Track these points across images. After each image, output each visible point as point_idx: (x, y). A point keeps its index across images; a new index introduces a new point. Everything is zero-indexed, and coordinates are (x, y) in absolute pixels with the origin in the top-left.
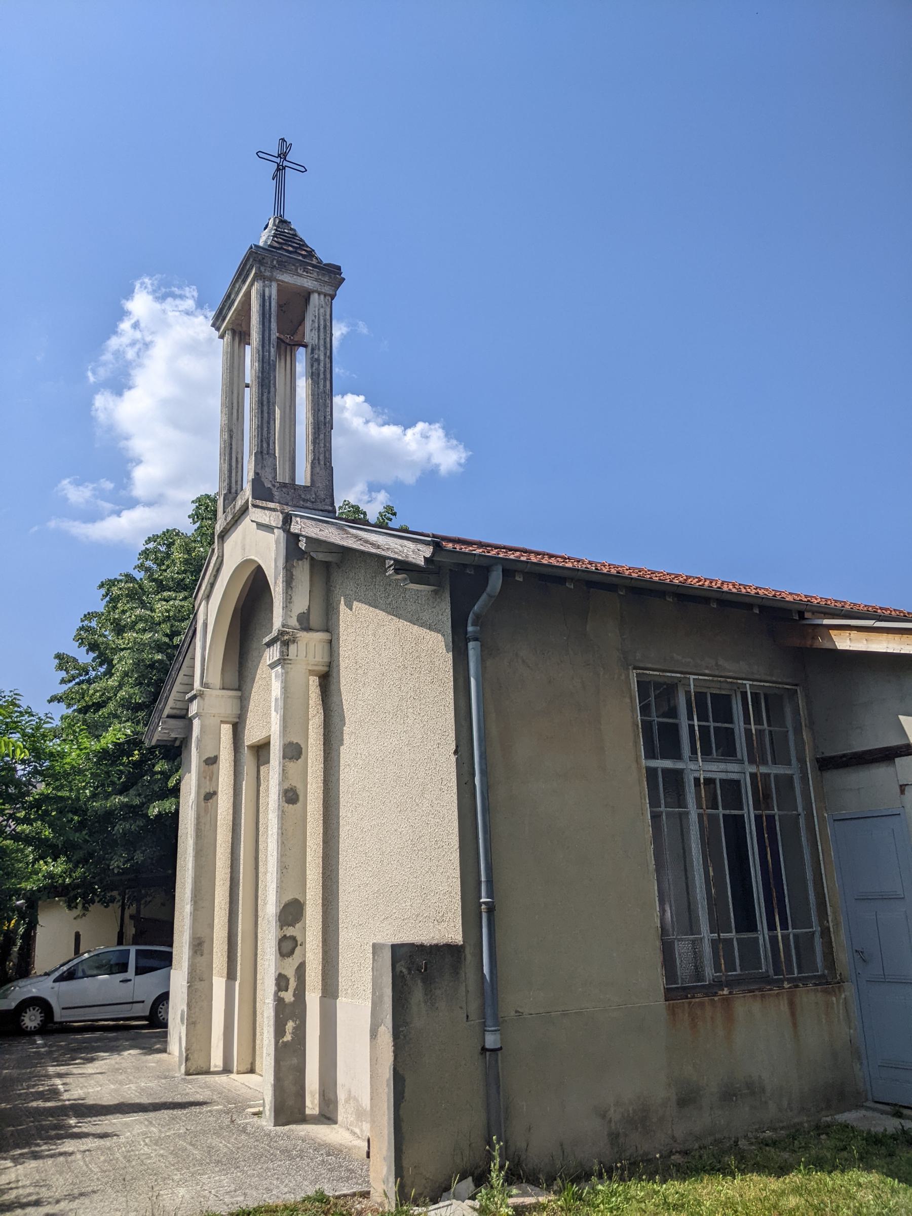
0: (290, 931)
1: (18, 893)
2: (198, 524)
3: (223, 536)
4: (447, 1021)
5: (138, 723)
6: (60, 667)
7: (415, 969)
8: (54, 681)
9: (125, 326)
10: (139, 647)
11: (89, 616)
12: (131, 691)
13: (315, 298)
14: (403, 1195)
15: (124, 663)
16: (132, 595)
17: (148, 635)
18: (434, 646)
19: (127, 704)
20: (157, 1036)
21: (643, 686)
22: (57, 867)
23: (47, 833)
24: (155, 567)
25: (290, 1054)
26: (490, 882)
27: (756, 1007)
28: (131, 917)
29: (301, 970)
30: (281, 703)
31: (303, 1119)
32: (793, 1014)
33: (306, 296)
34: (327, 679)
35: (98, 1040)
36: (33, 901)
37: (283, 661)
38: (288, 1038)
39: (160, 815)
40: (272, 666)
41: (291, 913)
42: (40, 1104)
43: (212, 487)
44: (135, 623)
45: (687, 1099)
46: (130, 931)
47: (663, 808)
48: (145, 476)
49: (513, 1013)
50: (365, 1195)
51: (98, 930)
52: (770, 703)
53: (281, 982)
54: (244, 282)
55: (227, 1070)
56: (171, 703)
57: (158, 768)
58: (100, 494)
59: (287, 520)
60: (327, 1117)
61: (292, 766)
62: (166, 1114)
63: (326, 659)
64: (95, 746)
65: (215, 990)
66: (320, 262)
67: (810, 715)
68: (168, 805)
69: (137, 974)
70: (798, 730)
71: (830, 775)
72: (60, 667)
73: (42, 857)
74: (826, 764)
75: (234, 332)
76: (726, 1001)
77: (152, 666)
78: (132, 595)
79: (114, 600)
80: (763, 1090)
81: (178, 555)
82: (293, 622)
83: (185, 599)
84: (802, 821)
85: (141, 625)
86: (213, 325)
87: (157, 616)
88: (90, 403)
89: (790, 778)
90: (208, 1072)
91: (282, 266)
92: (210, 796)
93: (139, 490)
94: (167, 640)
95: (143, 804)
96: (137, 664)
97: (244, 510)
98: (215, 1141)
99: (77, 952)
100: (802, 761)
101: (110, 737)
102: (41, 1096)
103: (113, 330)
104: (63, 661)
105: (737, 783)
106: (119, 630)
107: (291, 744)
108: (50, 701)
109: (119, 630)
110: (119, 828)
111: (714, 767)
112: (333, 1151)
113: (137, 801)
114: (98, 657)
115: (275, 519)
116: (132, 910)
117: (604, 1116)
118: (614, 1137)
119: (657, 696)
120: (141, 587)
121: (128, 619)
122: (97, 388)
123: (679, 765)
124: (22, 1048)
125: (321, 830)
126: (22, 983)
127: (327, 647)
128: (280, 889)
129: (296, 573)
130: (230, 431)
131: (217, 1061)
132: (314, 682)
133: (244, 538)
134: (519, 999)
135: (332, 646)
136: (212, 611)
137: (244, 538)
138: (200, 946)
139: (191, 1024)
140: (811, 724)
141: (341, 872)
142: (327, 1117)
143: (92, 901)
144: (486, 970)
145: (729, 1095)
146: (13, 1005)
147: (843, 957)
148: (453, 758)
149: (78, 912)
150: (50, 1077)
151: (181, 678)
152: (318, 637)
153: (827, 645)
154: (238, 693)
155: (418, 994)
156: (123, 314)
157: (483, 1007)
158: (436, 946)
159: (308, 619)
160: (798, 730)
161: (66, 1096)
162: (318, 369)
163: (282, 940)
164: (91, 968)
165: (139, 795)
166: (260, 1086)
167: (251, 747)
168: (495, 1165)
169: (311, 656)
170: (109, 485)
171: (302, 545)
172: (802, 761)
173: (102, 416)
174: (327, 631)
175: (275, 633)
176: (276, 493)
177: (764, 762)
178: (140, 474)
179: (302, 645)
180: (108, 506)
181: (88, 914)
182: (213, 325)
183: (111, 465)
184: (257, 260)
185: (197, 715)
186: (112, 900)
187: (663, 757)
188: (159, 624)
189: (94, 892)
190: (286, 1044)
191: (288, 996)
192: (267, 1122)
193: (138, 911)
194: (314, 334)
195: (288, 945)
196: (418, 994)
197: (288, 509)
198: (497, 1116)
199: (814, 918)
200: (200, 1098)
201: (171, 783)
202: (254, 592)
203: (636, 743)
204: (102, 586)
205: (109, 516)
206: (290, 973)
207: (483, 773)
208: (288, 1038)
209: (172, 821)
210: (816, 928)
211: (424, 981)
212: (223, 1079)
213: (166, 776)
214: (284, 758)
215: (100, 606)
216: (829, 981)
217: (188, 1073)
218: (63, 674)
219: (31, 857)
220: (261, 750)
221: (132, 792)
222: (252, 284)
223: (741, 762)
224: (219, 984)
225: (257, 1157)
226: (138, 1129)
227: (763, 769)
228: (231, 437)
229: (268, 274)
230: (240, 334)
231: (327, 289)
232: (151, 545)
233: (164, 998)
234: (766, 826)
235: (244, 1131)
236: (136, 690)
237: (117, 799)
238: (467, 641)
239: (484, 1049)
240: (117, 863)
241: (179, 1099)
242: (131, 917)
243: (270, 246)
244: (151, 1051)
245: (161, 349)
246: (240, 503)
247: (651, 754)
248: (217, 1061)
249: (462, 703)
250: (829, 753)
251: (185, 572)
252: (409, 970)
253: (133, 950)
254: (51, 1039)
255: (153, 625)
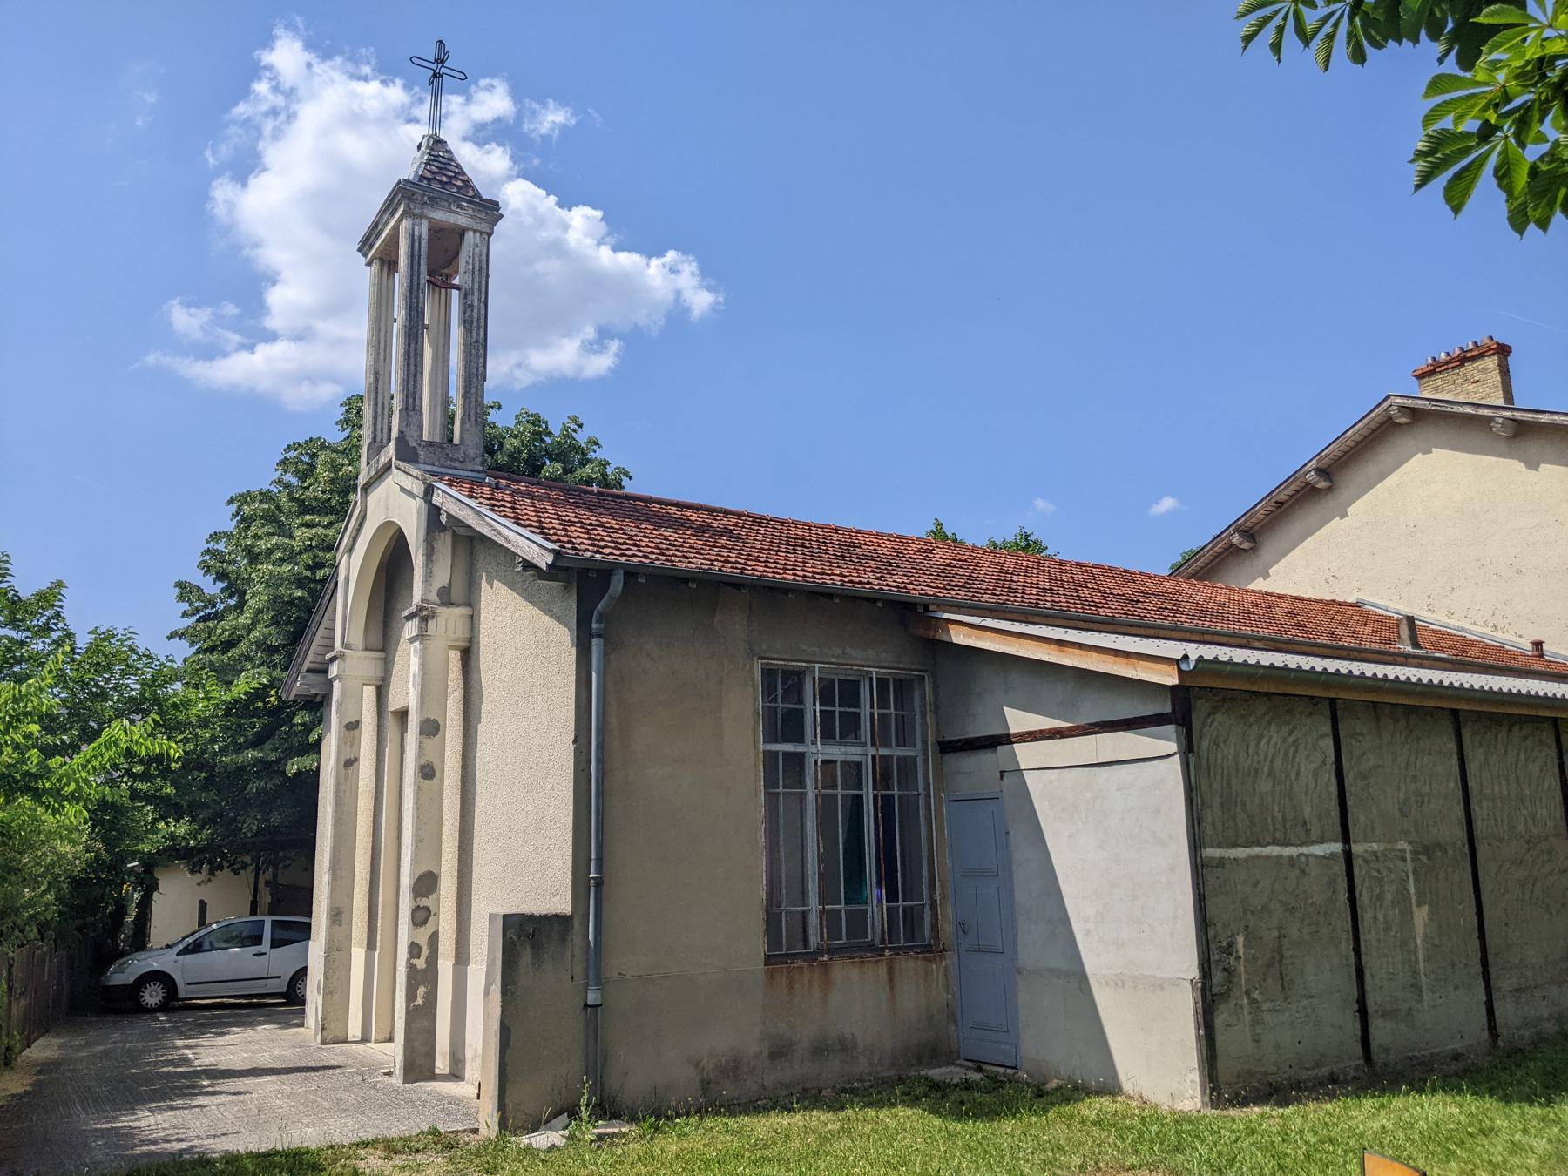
0: (423, 902)
1: (133, 855)
2: (347, 432)
3: (366, 488)
4: (557, 984)
5: (275, 667)
6: (182, 598)
7: (525, 936)
8: (175, 615)
9: (262, 87)
10: (274, 581)
11: (216, 537)
12: (266, 631)
13: (469, 236)
14: (503, 1124)
15: (257, 598)
16: (269, 518)
17: (286, 568)
18: (561, 639)
19: (261, 644)
20: (293, 1012)
21: (768, 673)
22: (181, 828)
23: (169, 790)
24: (295, 481)
25: (421, 1018)
26: (600, 859)
27: (854, 972)
28: (267, 883)
29: (434, 939)
30: (418, 680)
31: (433, 1077)
32: (891, 980)
33: (462, 232)
34: (468, 655)
35: (230, 1016)
36: (150, 864)
37: (422, 636)
38: (419, 1001)
39: (299, 772)
40: (412, 640)
41: (426, 884)
42: (172, 1069)
43: (362, 385)
44: (270, 552)
45: (780, 1051)
46: (266, 898)
47: (781, 789)
48: (287, 299)
49: (616, 975)
50: (475, 1131)
51: (228, 899)
52: (897, 689)
53: (414, 950)
54: (392, 214)
55: (365, 1039)
56: (310, 656)
57: (297, 720)
58: (218, 321)
59: (429, 490)
60: (456, 1075)
61: (428, 742)
62: (299, 1076)
63: (467, 635)
64: (227, 697)
65: (350, 959)
66: (477, 195)
67: (936, 699)
68: (307, 762)
69: (272, 946)
70: (924, 715)
71: (947, 757)
72: (182, 598)
73: (163, 818)
74: (948, 747)
75: (382, 261)
76: (825, 965)
77: (292, 602)
78: (269, 518)
79: (246, 522)
80: (855, 1046)
81: (323, 474)
82: (434, 597)
83: (330, 524)
84: (922, 802)
85: (278, 555)
86: (359, 250)
87: (297, 545)
88: (204, 196)
89: (914, 759)
90: (345, 1042)
91: (434, 202)
92: (351, 763)
93: (273, 322)
94: (308, 573)
95: (279, 760)
96: (275, 599)
97: (387, 468)
98: (345, 1095)
99: (202, 922)
100: (925, 742)
101: (242, 686)
102: (172, 1063)
103: (244, 93)
104: (185, 590)
105: (858, 765)
106: (254, 558)
107: (428, 720)
108: (169, 638)
109: (254, 558)
110: (253, 787)
111: (835, 749)
112: (454, 1100)
113: (273, 757)
114: (227, 588)
115: (418, 488)
116: (268, 875)
117: (697, 1066)
118: (705, 1084)
119: (782, 684)
120: (278, 508)
121: (263, 545)
122: (218, 172)
123: (800, 749)
124: (143, 1023)
125: (458, 804)
126: (141, 955)
127: (468, 621)
128: (415, 861)
129: (438, 545)
130: (377, 373)
131: (355, 1031)
132: (454, 656)
133: (387, 497)
134: (615, 965)
135: (473, 620)
136: (353, 567)
137: (387, 497)
138: (338, 916)
139: (328, 992)
140: (936, 709)
141: (475, 846)
142: (456, 1075)
143: (221, 868)
144: (591, 937)
145: (821, 1050)
146: (132, 980)
147: (948, 928)
148: (572, 747)
149: (199, 877)
150: (178, 1048)
151: (317, 641)
152: (459, 612)
153: (945, 638)
154: (382, 655)
155: (526, 957)
156: (256, 71)
157: (586, 970)
158: (546, 916)
159: (449, 594)
160: (924, 715)
161: (197, 1063)
162: (471, 317)
163: (416, 910)
164: (218, 940)
165: (276, 749)
166: (393, 1052)
167: (395, 713)
168: (583, 1101)
169: (451, 634)
170: (231, 309)
171: (443, 518)
172: (925, 742)
173: (220, 210)
174: (469, 605)
175: (413, 609)
176: (421, 452)
177: (886, 744)
178: (276, 297)
179: (441, 620)
180: (237, 338)
181: (215, 881)
182: (359, 250)
183: (240, 290)
184: (405, 195)
185: (337, 677)
186: (245, 866)
187: (785, 741)
188: (300, 553)
189: (224, 857)
190: (416, 1007)
191: (420, 963)
192: (397, 1081)
193: (275, 876)
194: (468, 277)
195: (422, 915)
196: (526, 957)
197: (430, 479)
198: (597, 1062)
199: (925, 892)
200: (334, 1063)
201: (313, 738)
202: (393, 565)
203: (755, 730)
204: (231, 501)
205: (237, 350)
206: (423, 942)
207: (600, 761)
208: (419, 1001)
209: (310, 781)
210: (927, 901)
211: (533, 947)
212: (361, 1047)
213: (308, 728)
214: (421, 733)
215: (230, 526)
216: (932, 951)
217: (323, 1043)
218: (186, 606)
219: (150, 818)
220: (402, 715)
221: (268, 745)
222: (400, 220)
223: (864, 745)
224: (358, 955)
225: (383, 1106)
226: (269, 1087)
227: (884, 751)
228: (377, 380)
229: (417, 211)
230: (387, 263)
231: (484, 227)
232: (291, 454)
233: (302, 973)
234: (885, 806)
235: (374, 1087)
236: (272, 630)
237: (251, 754)
238: (591, 637)
239: (586, 1005)
240: (251, 824)
241: (313, 1064)
242: (267, 883)
243: (422, 177)
244: (288, 1025)
245: (311, 116)
246: (383, 460)
247: (771, 737)
248: (355, 1031)
249: (584, 695)
250: (949, 738)
251: (331, 491)
252: (519, 937)
253: (268, 920)
254: (176, 1016)
255: (291, 556)
